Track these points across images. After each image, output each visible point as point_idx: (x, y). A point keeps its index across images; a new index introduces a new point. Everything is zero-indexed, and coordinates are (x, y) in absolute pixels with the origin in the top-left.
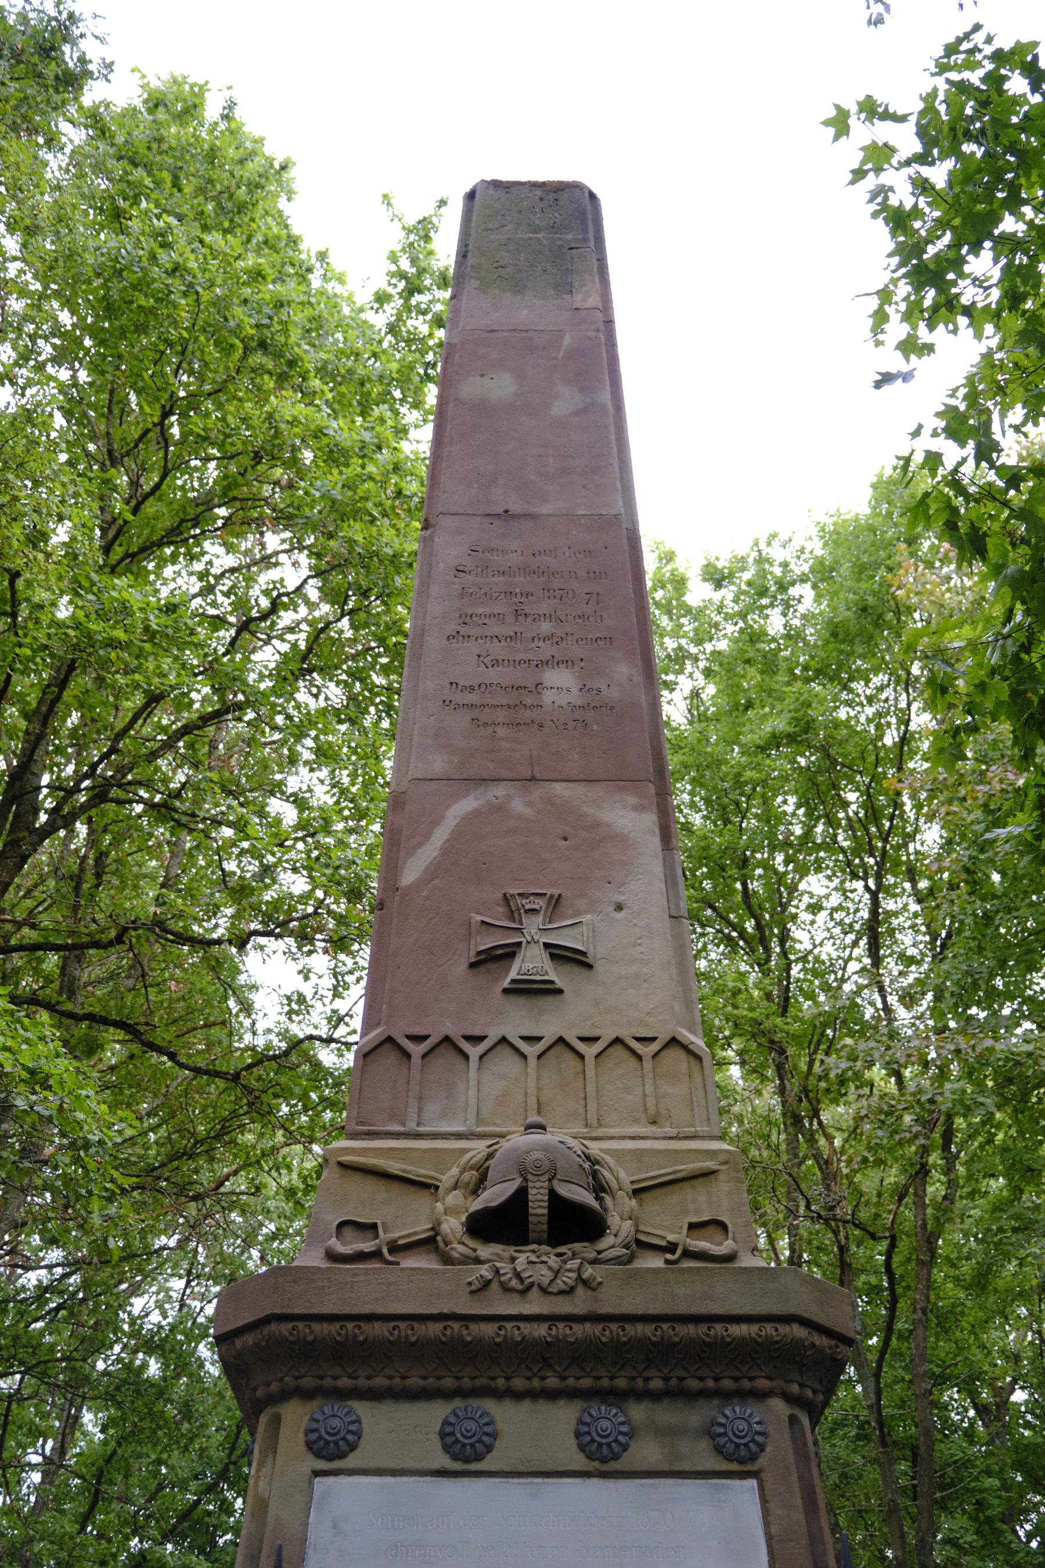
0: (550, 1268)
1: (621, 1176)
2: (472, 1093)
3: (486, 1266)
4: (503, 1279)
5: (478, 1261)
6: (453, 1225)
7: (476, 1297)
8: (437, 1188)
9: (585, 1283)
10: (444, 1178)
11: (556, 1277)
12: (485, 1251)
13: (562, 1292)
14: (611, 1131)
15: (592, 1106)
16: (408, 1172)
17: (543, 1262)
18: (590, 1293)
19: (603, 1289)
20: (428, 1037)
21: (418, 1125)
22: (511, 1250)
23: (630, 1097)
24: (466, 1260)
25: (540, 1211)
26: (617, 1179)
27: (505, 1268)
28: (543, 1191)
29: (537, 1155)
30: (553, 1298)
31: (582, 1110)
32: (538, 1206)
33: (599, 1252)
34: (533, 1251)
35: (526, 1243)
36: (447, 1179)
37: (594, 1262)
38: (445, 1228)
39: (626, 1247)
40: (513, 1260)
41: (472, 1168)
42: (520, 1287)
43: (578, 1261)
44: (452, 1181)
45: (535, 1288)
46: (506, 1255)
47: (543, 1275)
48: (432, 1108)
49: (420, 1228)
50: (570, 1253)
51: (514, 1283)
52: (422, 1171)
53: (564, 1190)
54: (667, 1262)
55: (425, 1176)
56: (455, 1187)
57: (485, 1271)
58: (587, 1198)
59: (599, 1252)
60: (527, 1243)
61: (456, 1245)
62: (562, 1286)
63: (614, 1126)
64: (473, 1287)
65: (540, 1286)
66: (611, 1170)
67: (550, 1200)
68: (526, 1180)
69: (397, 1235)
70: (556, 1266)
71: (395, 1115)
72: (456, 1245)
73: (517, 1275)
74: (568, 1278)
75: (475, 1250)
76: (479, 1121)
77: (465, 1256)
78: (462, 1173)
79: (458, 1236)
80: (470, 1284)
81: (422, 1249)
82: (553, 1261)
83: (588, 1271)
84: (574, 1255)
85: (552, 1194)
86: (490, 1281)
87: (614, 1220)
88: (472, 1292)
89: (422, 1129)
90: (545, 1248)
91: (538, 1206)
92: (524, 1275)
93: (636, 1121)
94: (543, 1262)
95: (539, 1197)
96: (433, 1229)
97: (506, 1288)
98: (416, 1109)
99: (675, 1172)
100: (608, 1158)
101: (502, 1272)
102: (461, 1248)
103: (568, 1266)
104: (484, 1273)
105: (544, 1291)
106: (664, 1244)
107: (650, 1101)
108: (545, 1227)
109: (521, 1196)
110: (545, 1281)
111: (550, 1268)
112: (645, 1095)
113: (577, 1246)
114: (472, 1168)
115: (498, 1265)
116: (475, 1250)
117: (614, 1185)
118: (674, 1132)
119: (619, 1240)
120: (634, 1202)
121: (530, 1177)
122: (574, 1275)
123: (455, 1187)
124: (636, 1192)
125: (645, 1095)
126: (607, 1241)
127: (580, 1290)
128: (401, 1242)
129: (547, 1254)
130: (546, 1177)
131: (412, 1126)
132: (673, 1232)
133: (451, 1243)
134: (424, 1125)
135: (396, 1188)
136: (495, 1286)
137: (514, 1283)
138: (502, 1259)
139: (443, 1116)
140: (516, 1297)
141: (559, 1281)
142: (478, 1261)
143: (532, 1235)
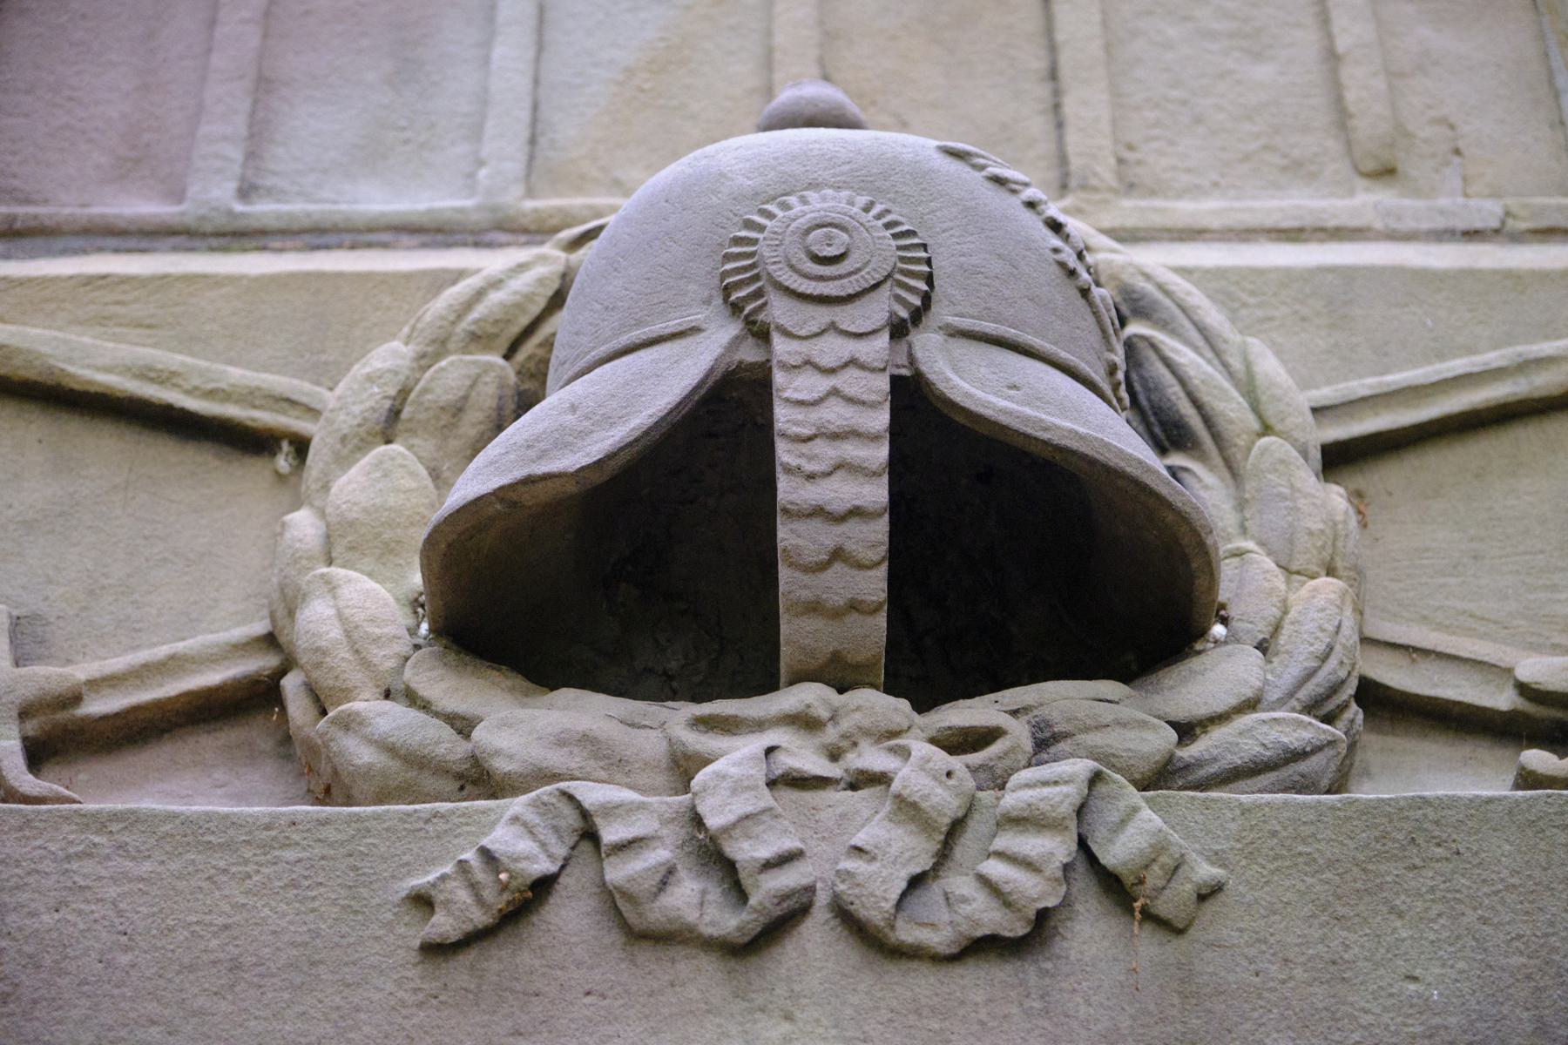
0: (908, 810)
1: (1275, 378)
2: (510, 51)
3: (517, 805)
4: (618, 872)
5: (479, 780)
6: (368, 607)
7: (458, 972)
8: (301, 446)
9: (1116, 888)
10: (329, 399)
11: (944, 854)
12: (522, 724)
13: (982, 947)
14: (1186, 210)
15: (1087, 105)
16: (167, 378)
17: (862, 780)
18: (1149, 946)
19: (1225, 925)
20: (478, 271)
21: (246, 191)
22: (676, 720)
23: (1263, 72)
24: (413, 775)
25: (841, 492)
26: (1249, 388)
27: (633, 810)
28: (851, 382)
29: (820, 204)
30: (923, 982)
31: (1038, 125)
32: (832, 474)
33: (1186, 730)
34: (805, 722)
35: (761, 676)
36: (349, 398)
37: (1161, 777)
38: (317, 621)
39: (1321, 708)
40: (684, 767)
41: (478, 339)
42: (727, 921)
43: (1081, 767)
44: (375, 399)
45: (816, 932)
46: (650, 745)
47: (869, 852)
48: (315, 127)
49: (205, 644)
50: (1019, 733)
51: (691, 899)
52: (237, 375)
53: (979, 384)
54: (1529, 779)
55: (249, 396)
56: (390, 425)
57: (516, 835)
58: (1112, 434)
59: (1186, 730)
60: (767, 683)
61: (366, 705)
62: (988, 917)
63: (1195, 191)
64: (443, 925)
65: (848, 919)
66: (1209, 340)
67: (897, 431)
68: (761, 333)
69: (81, 672)
70: (944, 801)
71: (135, 161)
72: (366, 705)
73: (713, 857)
74: (1026, 868)
75: (463, 725)
76: (534, 171)
77: (416, 761)
78: (425, 360)
79: (384, 658)
80: (423, 902)
81: (209, 743)
82: (924, 771)
83: (1136, 830)
84: (1046, 742)
85: (913, 399)
86: (543, 886)
87: (1247, 579)
88: (436, 950)
89: (263, 210)
90: (875, 704)
91: (832, 474)
92: (747, 851)
93: (1298, 169)
94: (862, 780)
95: (835, 414)
96: (270, 641)
97: (642, 934)
98: (239, 125)
99: (1525, 366)
100: (1196, 298)
101: (611, 833)
102: (391, 718)
103: (1013, 799)
104: (503, 839)
105: (870, 939)
106: (1503, 700)
107: (1362, 84)
108: (874, 585)
109: (727, 423)
110: (878, 886)
111: (908, 810)
112: (1332, 57)
113: (1061, 698)
114: (478, 339)
115: (592, 794)
116: (463, 725)
117: (1232, 408)
118: (1487, 212)
119: (1287, 669)
120: (1335, 497)
121: (779, 311)
122: (1055, 848)
123: (390, 425)
124: (1338, 459)
125: (1332, 57)
126: (1217, 675)
127: (1091, 933)
128: (96, 706)
129: (888, 735)
130: (877, 310)
131: (214, 194)
132: (1536, 648)
133: (347, 694)
134: (271, 192)
135: (105, 451)
136: (570, 916)
137: (691, 899)
138: (614, 765)
139: (369, 157)
140: (701, 976)
141: (959, 883)
142: (479, 780)
143: (797, 635)
